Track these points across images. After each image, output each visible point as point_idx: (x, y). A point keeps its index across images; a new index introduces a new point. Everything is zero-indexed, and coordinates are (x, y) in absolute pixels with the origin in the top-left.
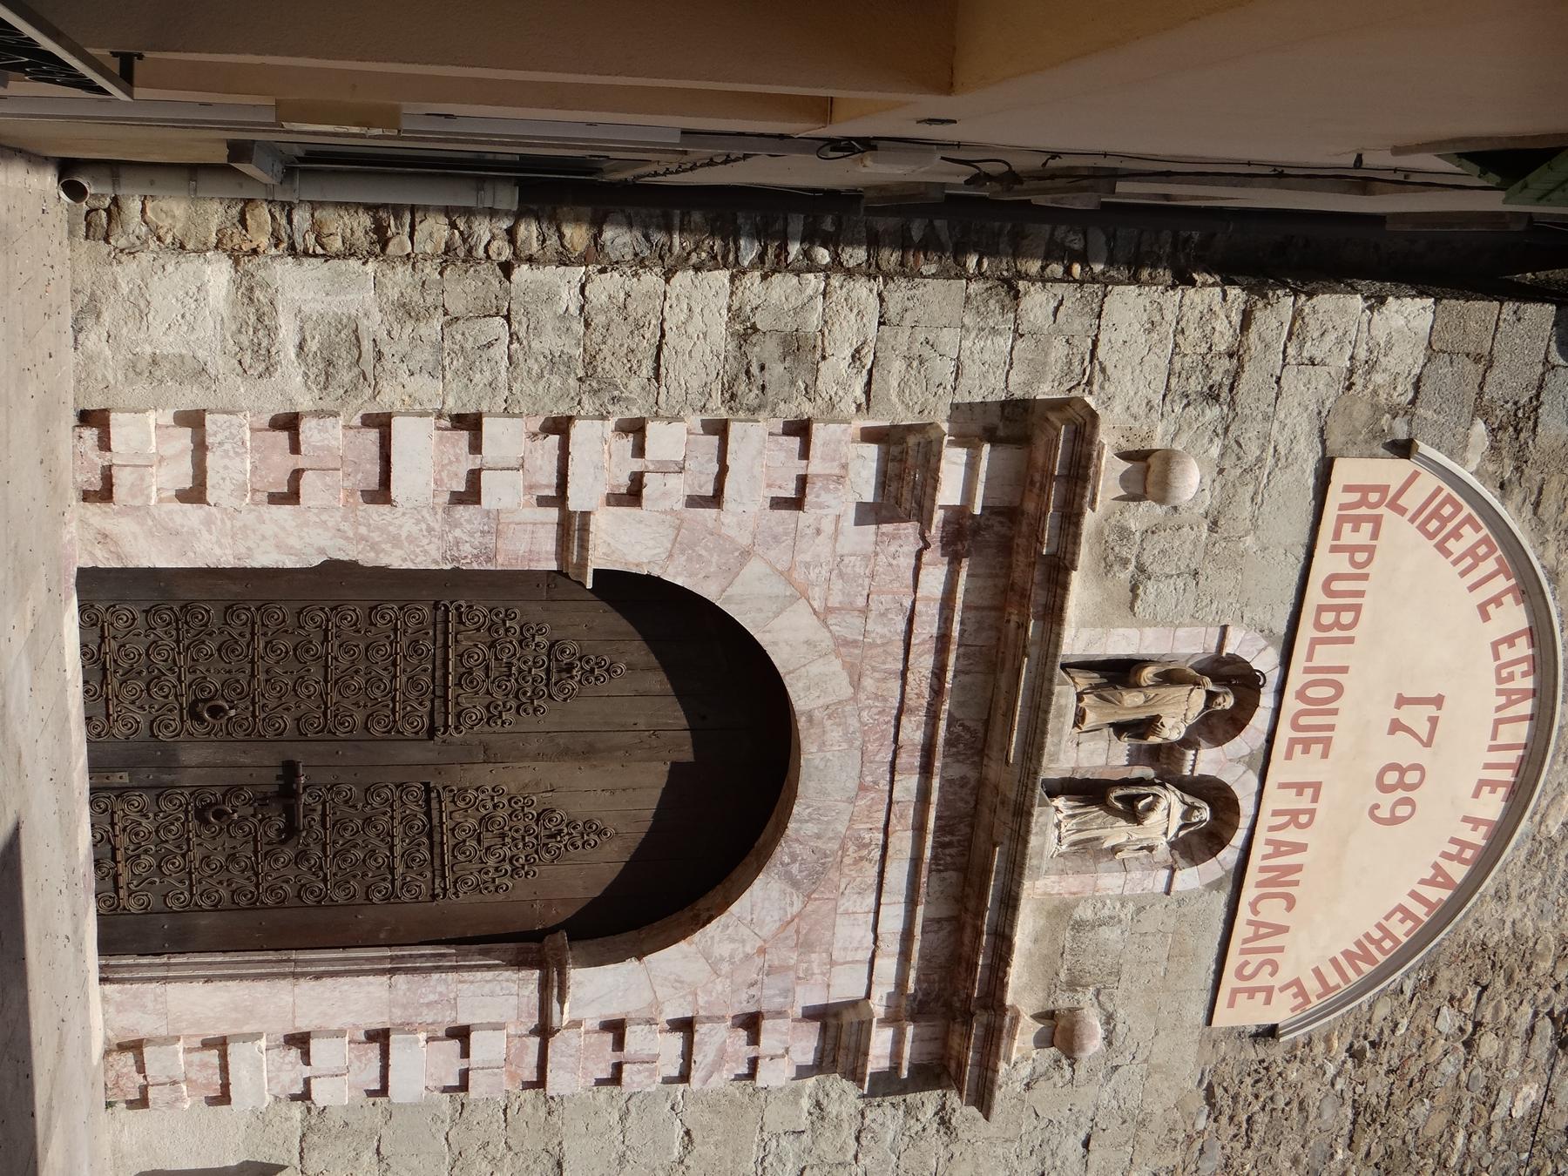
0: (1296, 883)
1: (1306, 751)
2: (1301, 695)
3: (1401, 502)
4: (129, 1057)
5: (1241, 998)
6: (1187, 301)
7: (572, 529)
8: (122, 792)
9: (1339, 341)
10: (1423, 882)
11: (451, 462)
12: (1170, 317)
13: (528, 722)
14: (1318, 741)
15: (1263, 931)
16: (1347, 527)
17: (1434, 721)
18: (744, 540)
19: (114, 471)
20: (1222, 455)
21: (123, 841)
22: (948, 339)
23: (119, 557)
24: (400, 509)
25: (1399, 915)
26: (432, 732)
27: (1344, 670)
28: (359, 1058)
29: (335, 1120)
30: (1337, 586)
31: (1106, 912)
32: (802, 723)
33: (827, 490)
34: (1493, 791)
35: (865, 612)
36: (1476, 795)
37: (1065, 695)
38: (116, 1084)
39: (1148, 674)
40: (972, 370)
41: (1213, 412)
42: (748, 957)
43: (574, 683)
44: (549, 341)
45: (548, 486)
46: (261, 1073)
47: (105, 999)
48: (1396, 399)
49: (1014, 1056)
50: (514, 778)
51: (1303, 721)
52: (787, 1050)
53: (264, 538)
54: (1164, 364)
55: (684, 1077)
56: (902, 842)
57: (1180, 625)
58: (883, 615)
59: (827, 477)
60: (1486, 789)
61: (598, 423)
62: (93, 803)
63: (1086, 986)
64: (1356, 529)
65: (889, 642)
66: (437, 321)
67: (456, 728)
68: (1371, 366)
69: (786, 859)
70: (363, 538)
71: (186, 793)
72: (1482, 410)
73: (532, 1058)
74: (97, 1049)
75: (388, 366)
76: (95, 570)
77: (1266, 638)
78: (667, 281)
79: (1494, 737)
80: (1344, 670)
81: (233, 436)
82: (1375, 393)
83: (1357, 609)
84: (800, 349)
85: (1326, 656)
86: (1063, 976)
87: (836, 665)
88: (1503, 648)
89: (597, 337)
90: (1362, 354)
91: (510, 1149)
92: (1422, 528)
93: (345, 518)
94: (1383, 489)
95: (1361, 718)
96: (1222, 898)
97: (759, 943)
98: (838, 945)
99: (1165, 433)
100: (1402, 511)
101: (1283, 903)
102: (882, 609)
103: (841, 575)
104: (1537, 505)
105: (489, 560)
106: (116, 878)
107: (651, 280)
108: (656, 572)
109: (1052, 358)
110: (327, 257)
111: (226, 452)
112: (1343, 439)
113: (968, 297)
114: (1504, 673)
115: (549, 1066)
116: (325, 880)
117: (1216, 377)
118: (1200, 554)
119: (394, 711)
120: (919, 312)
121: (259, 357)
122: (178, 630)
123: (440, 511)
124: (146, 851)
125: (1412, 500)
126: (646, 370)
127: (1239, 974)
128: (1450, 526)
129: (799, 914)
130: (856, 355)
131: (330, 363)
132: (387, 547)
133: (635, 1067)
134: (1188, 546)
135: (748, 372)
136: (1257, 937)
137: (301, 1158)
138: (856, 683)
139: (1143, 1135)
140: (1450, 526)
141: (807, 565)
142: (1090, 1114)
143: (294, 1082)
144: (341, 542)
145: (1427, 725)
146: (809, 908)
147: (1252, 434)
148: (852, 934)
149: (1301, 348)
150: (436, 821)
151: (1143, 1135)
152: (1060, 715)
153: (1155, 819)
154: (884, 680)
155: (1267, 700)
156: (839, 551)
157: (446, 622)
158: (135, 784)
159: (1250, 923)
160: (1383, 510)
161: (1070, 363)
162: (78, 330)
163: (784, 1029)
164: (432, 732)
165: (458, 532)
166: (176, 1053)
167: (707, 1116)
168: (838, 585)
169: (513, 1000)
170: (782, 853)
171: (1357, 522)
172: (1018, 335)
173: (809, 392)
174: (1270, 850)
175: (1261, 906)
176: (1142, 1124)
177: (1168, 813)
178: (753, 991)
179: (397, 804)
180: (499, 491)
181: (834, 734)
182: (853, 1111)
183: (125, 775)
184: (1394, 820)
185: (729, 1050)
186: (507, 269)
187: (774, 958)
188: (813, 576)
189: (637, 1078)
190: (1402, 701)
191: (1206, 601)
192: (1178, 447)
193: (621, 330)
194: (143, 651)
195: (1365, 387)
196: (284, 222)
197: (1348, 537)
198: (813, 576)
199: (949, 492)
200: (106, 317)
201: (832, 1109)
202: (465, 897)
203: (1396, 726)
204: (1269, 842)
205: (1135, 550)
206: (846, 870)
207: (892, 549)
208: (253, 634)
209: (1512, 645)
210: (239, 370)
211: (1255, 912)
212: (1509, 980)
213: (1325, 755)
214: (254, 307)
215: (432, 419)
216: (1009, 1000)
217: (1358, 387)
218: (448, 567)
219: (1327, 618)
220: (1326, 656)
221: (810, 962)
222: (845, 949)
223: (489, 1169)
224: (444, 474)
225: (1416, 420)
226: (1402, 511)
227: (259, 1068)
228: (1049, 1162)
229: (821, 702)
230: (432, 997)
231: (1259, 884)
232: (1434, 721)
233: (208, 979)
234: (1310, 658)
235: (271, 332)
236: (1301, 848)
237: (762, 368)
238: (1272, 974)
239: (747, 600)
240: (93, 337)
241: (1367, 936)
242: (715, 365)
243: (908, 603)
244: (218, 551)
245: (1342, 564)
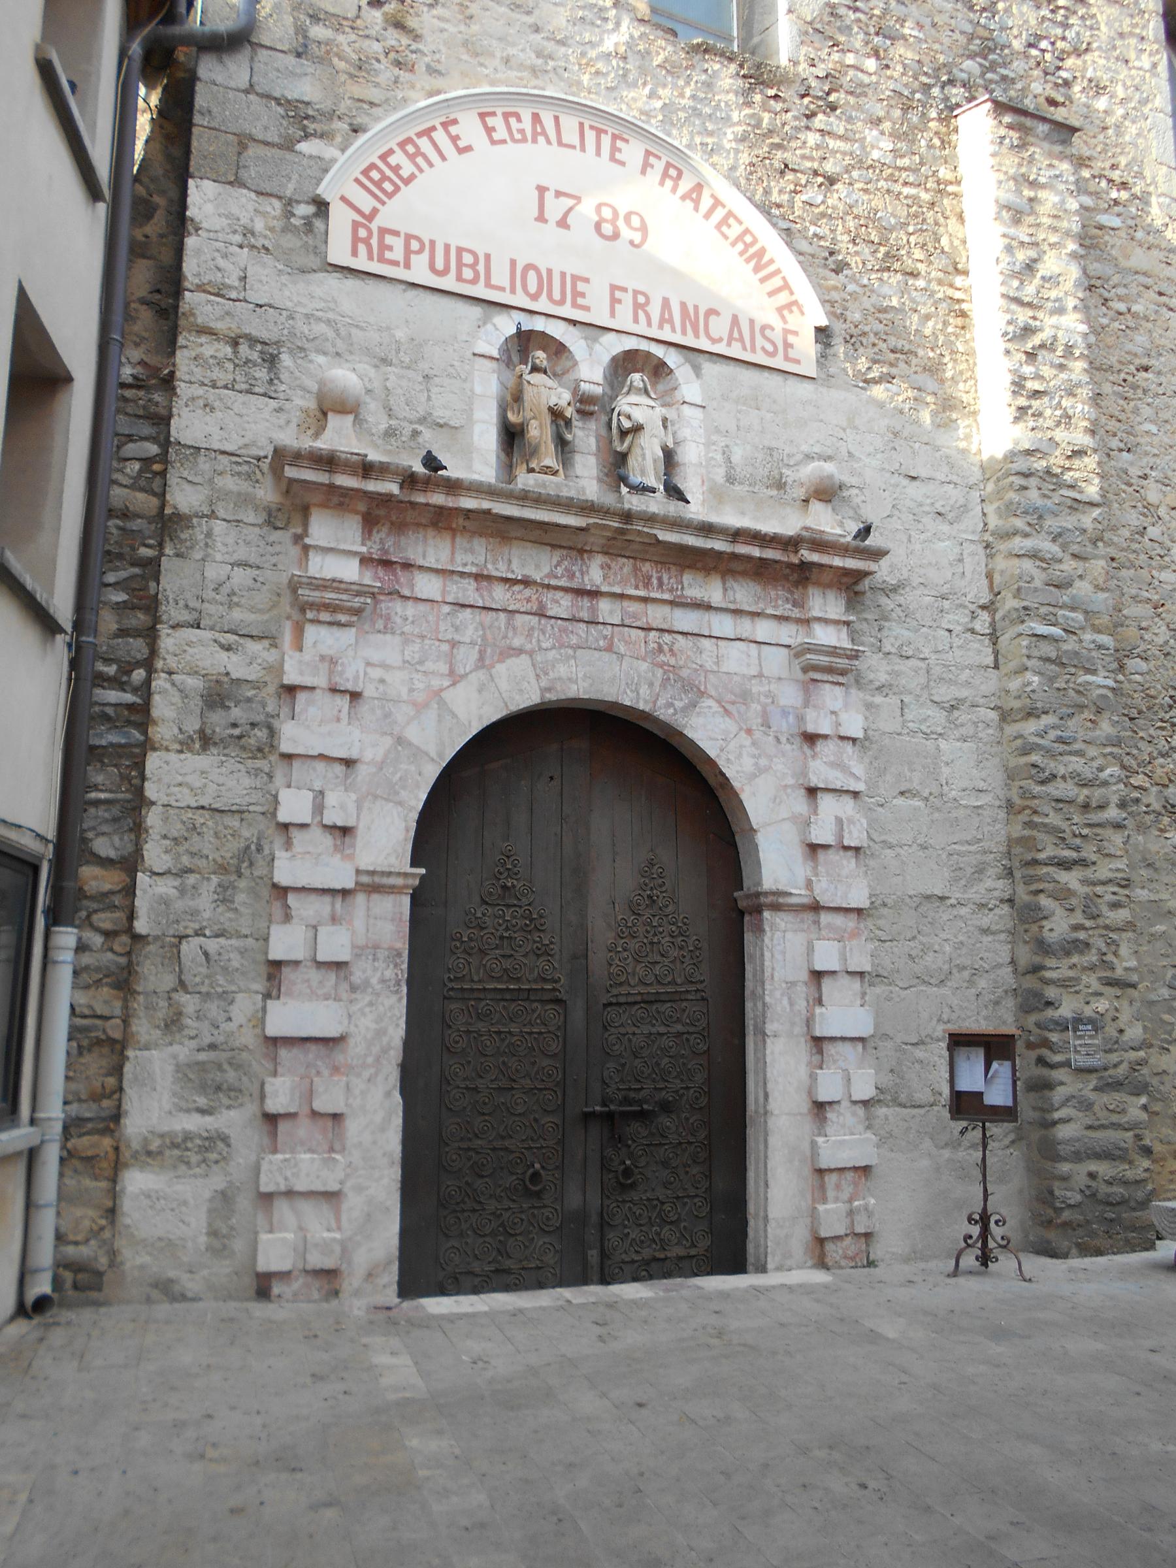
0: (696, 308)
1: (583, 295)
2: (535, 297)
3: (367, 211)
4: (829, 1247)
5: (792, 353)
6: (187, 378)
7: (372, 885)
8: (604, 1255)
9: (225, 256)
10: (696, 209)
11: (310, 987)
12: (200, 391)
14: (574, 287)
15: (736, 335)
16: (388, 255)
17: (559, 194)
18: (388, 741)
19: (309, 1267)
20: (325, 354)
21: (647, 1253)
22: (213, 572)
23: (389, 1263)
24: (352, 1028)
25: (724, 229)
26: (558, 1001)
27: (513, 263)
28: (835, 1061)
29: (887, 1080)
30: (440, 265)
31: (719, 457)
32: (551, 696)
33: (342, 673)
34: (620, 150)
35: (454, 644)
36: (623, 164)
37: (525, 480)
38: (852, 1259)
39: (512, 417)
40: (242, 554)
41: (286, 360)
42: (754, 744)
43: (519, 885)
44: (205, 902)
45: (333, 905)
46: (846, 1142)
47: (779, 1269)
48: (278, 212)
49: (839, 531)
50: (601, 932)
51: (557, 295)
52: (833, 713)
53: (375, 1143)
54: (241, 398)
55: (856, 794)
56: (656, 615)
57: (472, 391)
58: (457, 629)
59: (331, 672)
60: (618, 156)
61: (276, 863)
62: (609, 1283)
63: (781, 474)
64: (390, 248)
65: (482, 624)
66: (182, 997)
67: (556, 982)
68: (248, 232)
69: (671, 711)
70: (378, 1059)
71: (607, 1202)
72: (288, 145)
73: (838, 920)
74: (820, 1277)
75: (222, 1039)
76: (401, 1284)
77: (485, 323)
78: (153, 803)
79: (574, 147)
80: (513, 263)
81: (280, 1169)
82: (272, 229)
83: (460, 250)
84: (218, 694)
85: (501, 276)
86: (774, 492)
87: (500, 668)
88: (496, 136)
89: (202, 863)
90: (238, 238)
91: (914, 938)
92: (390, 196)
93: (359, 1075)
94: (356, 225)
95: (550, 250)
96: (708, 367)
97: (743, 734)
98: (745, 671)
99: (303, 397)
100: (375, 211)
101: (712, 318)
102: (451, 629)
103: (421, 662)
104: (372, 104)
105: (399, 955)
106: (680, 1258)
107: (153, 818)
108: (416, 816)
109: (235, 488)
110: (121, 1089)
111: (293, 1174)
112: (312, 257)
113: (177, 555)
114: (518, 136)
115: (844, 905)
116: (688, 1088)
117: (255, 356)
118: (410, 374)
119: (540, 1033)
120: (188, 595)
121: (213, 1146)
122: (463, 1211)
123: (354, 996)
124: (658, 1234)
125: (366, 203)
126: (233, 822)
127: (772, 354)
128: (388, 173)
129: (719, 702)
130: (228, 648)
131: (219, 1088)
132: (385, 1040)
133: (846, 835)
134: (404, 383)
135: (240, 737)
136: (741, 339)
137: (919, 1106)
138: (520, 651)
139: (905, 434)
140: (388, 173)
141: (411, 690)
142: (888, 475)
143: (854, 1114)
144: (380, 1078)
145: (562, 199)
146: (713, 693)
147: (305, 329)
148: (736, 659)
149: (230, 287)
150: (639, 998)
151: (905, 434)
152: (544, 485)
153: (639, 415)
154: (514, 629)
155: (539, 324)
156: (400, 663)
157: (462, 989)
159: (729, 344)
160: (374, 226)
161: (239, 474)
162: (183, 1298)
163: (814, 714)
164: (558, 1001)
165: (374, 981)
166: (827, 1211)
167: (888, 777)
168: (429, 666)
169: (789, 935)
170: (664, 714)
171: (383, 247)
172: (213, 515)
173: (257, 685)
174: (667, 327)
175: (715, 335)
176: (896, 434)
177: (635, 406)
178: (783, 740)
179: (622, 1030)
180: (335, 944)
181: (562, 670)
182: (884, 662)
183: (590, 1252)
184: (644, 229)
185: (832, 758)
186: (137, 938)
187: (755, 722)
188: (421, 686)
189: (855, 834)
190: (541, 218)
191: (451, 370)
192: (315, 388)
193: (196, 843)
194: (481, 1240)
195: (265, 237)
196: (90, 1125)
197: (397, 254)
198: (421, 686)
199: (349, 571)
200: (172, 1274)
201: (883, 677)
203: (563, 223)
204: (661, 327)
205: (406, 424)
206: (681, 663)
207: (398, 620)
208: (469, 1149)
209: (494, 129)
210: (222, 1164)
211: (720, 340)
212: (779, 146)
213: (587, 280)
214: (172, 1151)
215: (269, 1002)
216: (791, 533)
217: (267, 243)
218: (405, 989)
219: (468, 274)
220: (501, 276)
221: (759, 693)
222: (748, 665)
223: (931, 954)
224: (320, 992)
225: (296, 197)
226: (375, 211)
227: (842, 1142)
228: (927, 509)
229: (533, 681)
230: (785, 1002)
231: (697, 336)
232: (559, 194)
233: (767, 1185)
234: (503, 289)
235: (188, 1136)
236: (666, 303)
237: (234, 725)
238: (773, 329)
239: (439, 741)
240: (189, 1285)
241: (741, 253)
242: (231, 764)
243: (446, 609)
244: (385, 1181)
245: (420, 263)
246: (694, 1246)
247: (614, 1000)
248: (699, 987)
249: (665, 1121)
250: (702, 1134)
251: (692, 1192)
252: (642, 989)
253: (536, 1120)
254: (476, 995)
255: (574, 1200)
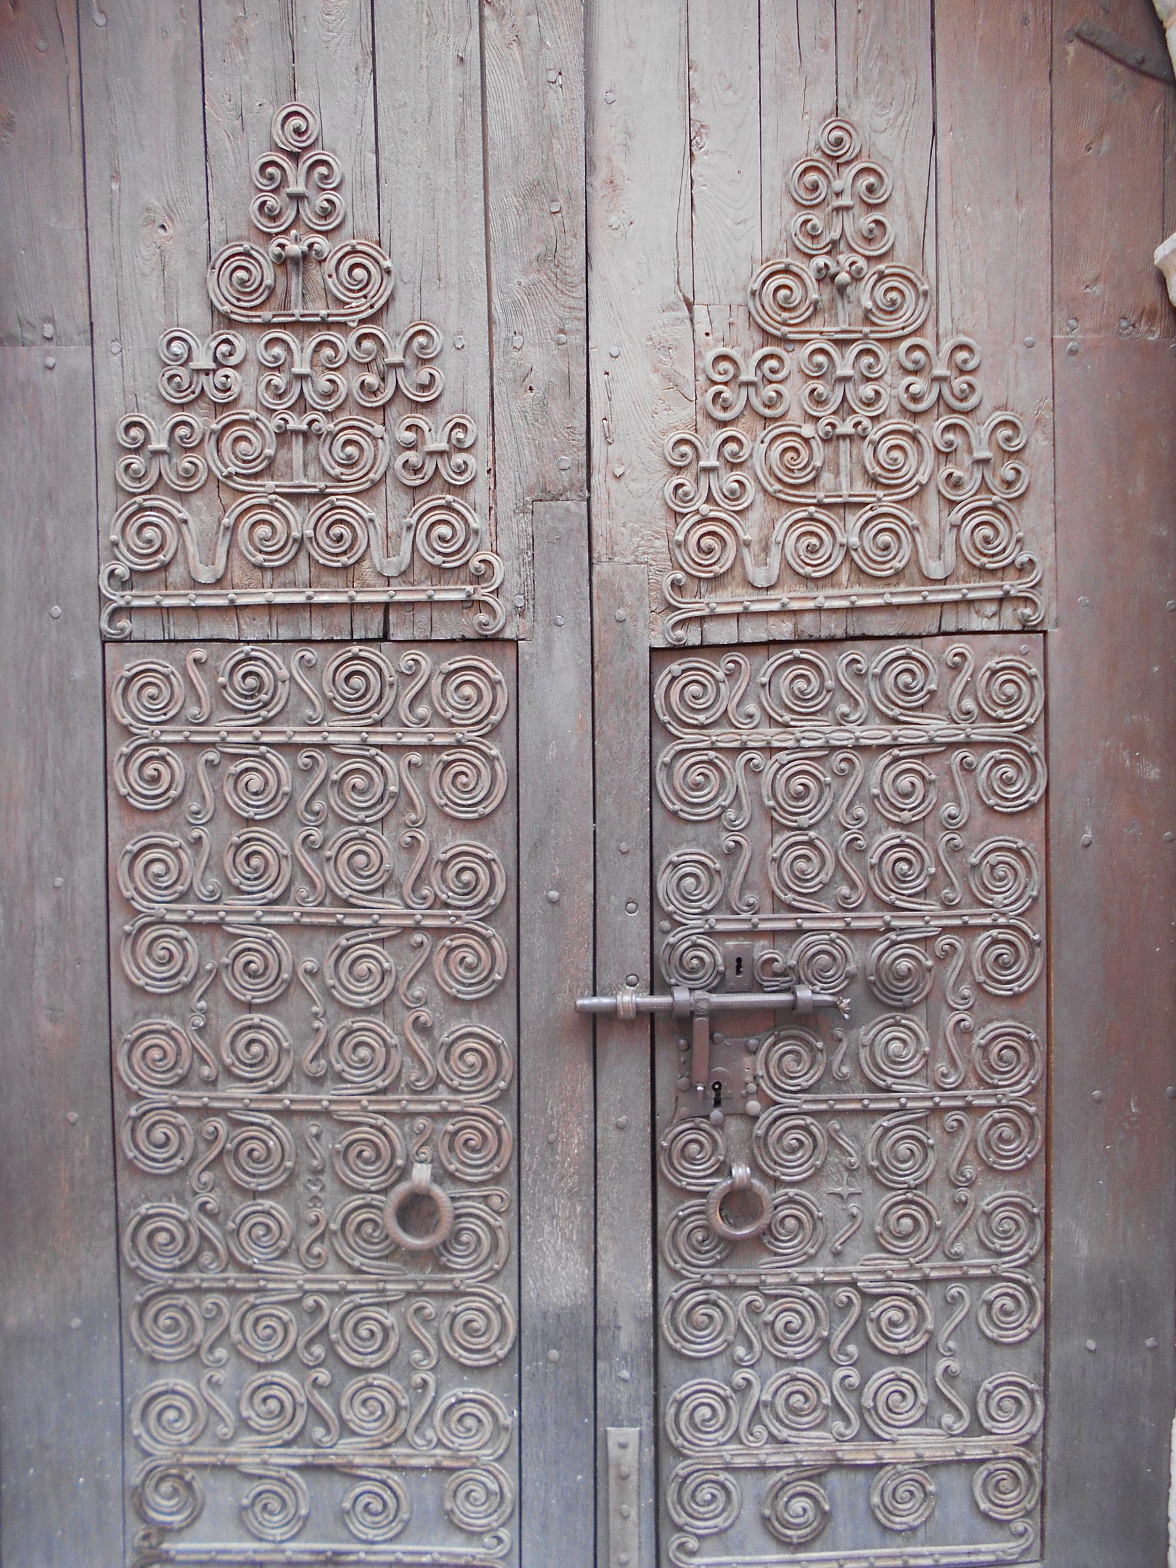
13: (459, 376)
150: (784, 629)
158: (645, 1412)
179: (725, 737)
183: (615, 1435)
202: (1035, 534)
208: (206, 1111)
246: (976, 1428)
247: (692, 637)
248: (1014, 585)
249: (891, 1040)
250: (1017, 1086)
251: (978, 1263)
252: (790, 596)
253: (423, 1029)
254: (208, 629)
255: (557, 1275)
